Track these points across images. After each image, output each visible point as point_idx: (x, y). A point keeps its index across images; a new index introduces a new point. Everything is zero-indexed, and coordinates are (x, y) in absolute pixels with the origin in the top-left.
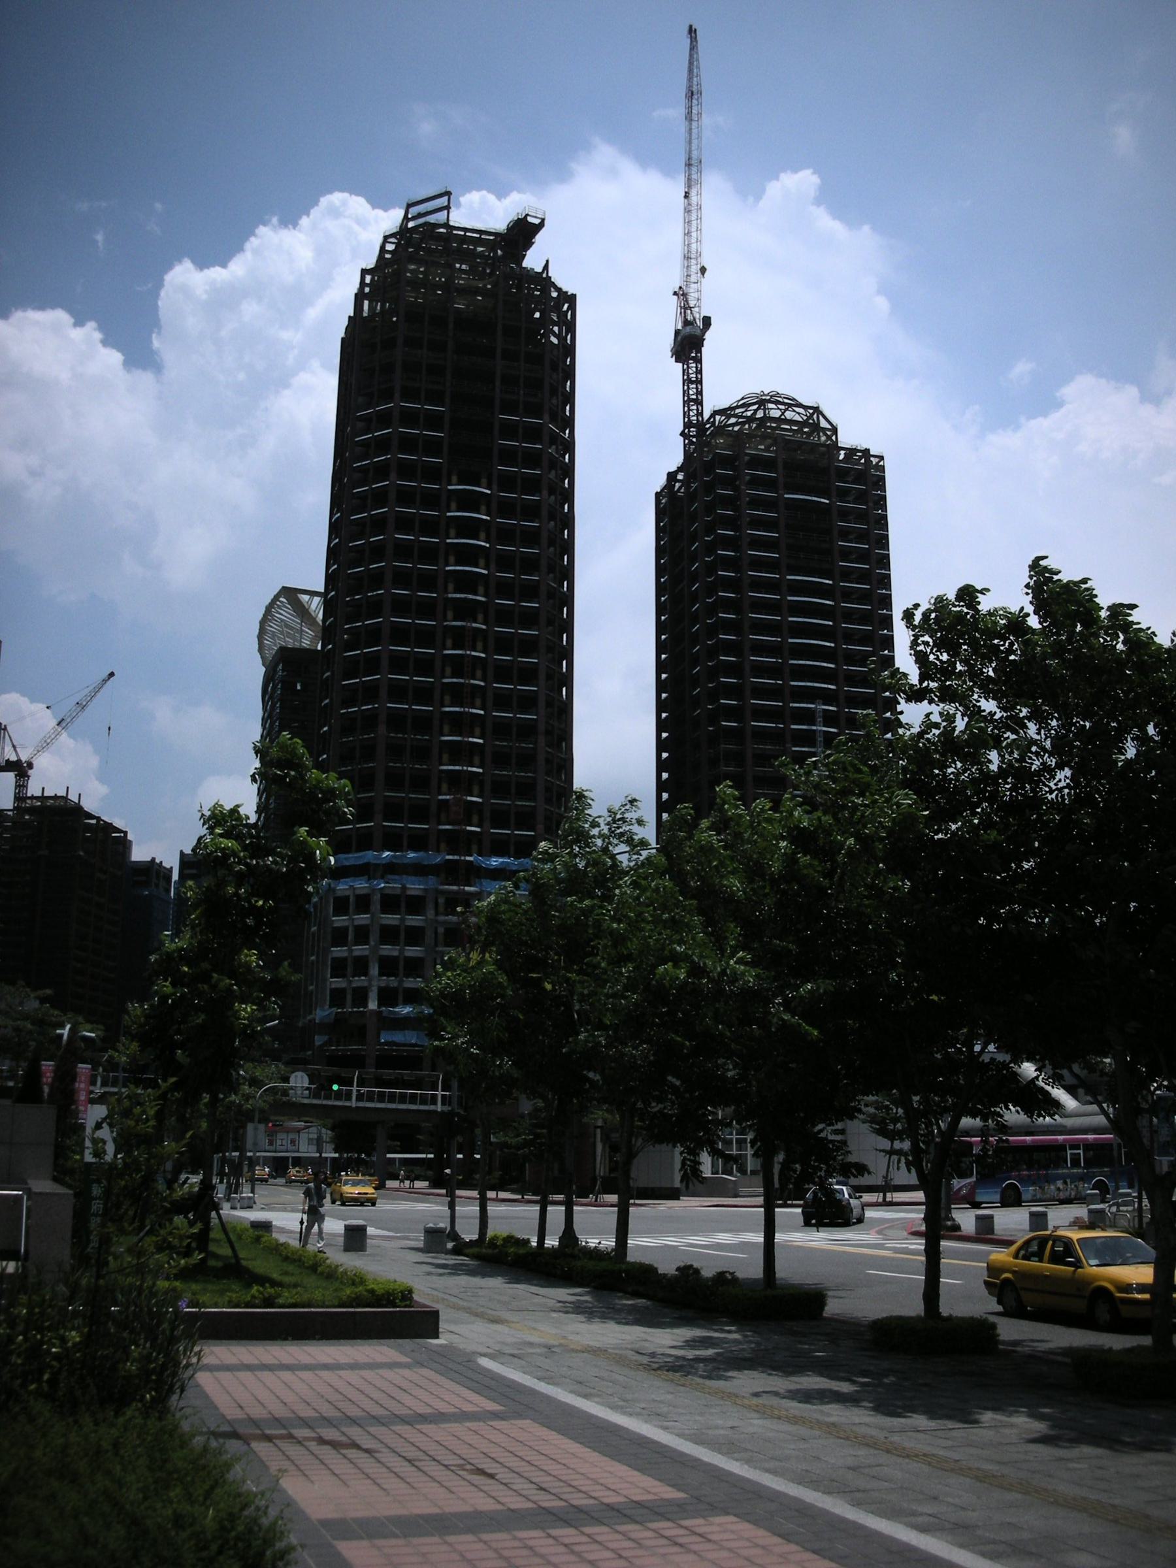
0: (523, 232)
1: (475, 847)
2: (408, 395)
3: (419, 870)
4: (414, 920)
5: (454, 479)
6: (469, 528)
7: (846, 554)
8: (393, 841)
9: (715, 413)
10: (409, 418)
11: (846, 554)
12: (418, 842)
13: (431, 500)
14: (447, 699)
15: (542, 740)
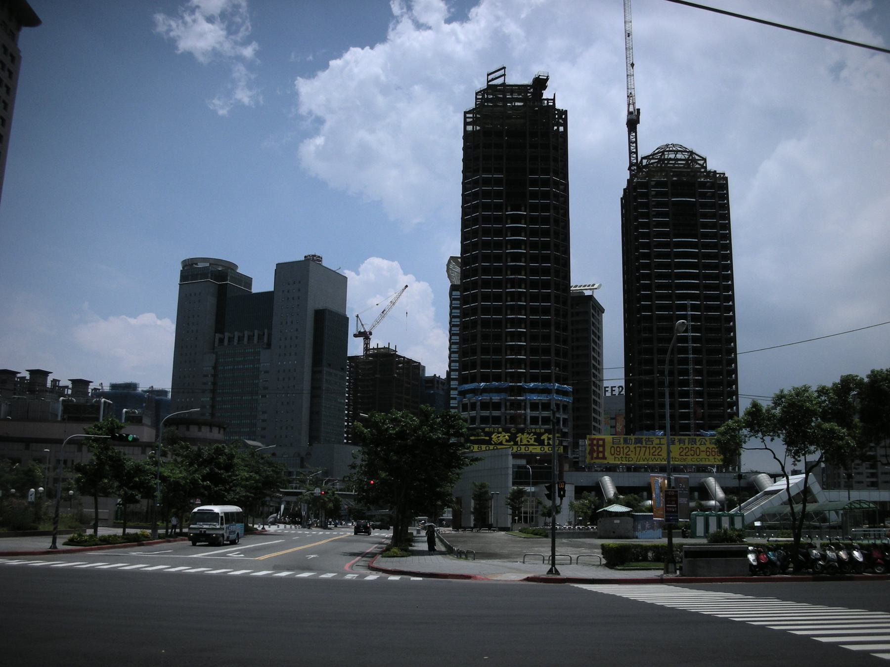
0: (540, 83)
1: (523, 379)
2: (486, 171)
3: (498, 390)
4: (496, 413)
5: (509, 209)
6: (516, 232)
7: (705, 225)
8: (485, 378)
9: (643, 158)
10: (486, 182)
11: (705, 225)
12: (497, 378)
13: (498, 220)
14: (509, 312)
15: (553, 328)
